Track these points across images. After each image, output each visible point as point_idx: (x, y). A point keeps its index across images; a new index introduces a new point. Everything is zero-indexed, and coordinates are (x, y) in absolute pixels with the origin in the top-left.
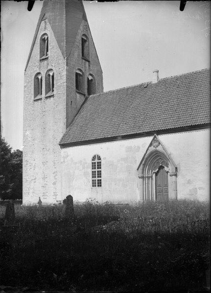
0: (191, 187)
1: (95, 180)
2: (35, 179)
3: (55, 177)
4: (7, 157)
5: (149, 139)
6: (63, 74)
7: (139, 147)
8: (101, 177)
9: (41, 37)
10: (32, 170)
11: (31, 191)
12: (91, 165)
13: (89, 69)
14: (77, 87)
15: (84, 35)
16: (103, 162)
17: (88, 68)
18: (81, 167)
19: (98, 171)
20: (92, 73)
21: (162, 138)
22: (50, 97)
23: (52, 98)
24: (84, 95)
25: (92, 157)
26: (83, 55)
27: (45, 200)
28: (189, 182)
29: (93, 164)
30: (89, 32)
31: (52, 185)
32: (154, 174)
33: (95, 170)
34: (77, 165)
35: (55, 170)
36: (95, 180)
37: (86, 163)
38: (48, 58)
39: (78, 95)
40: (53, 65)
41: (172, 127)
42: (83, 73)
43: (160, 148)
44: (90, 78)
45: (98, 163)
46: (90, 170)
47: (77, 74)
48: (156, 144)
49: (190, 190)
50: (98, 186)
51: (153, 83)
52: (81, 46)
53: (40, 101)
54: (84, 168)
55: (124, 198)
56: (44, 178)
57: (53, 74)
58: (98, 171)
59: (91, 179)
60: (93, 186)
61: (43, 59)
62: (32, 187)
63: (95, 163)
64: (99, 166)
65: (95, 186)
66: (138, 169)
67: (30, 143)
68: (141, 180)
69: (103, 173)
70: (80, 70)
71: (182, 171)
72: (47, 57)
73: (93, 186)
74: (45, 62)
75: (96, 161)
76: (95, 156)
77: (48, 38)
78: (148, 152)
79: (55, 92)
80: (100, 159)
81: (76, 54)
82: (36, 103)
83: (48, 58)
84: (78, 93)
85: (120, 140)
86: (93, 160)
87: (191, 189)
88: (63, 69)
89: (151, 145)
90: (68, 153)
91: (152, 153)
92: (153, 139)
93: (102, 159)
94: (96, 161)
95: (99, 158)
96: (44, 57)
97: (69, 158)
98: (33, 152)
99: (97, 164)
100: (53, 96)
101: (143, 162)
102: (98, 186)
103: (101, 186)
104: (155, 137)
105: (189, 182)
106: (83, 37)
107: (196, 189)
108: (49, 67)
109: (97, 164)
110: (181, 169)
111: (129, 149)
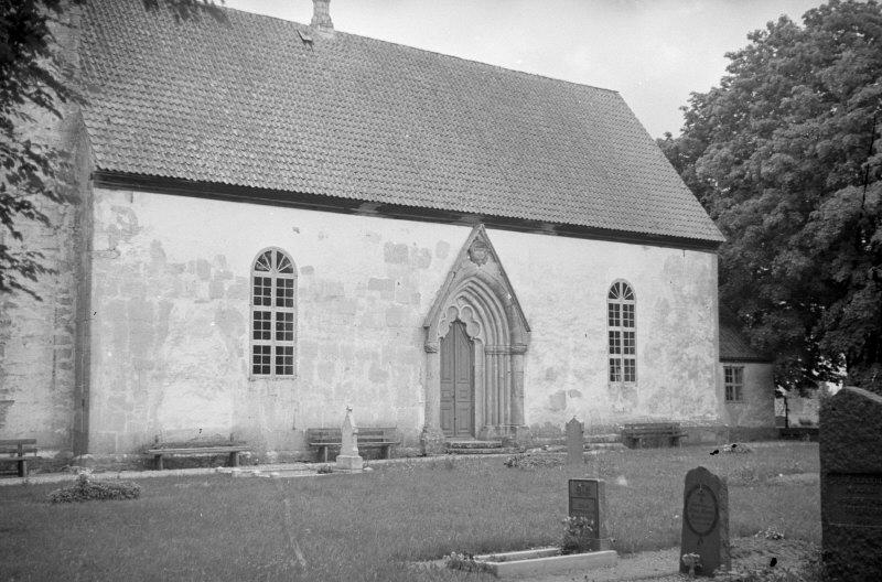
4: (799, 278)
8: (290, 337)
12: (249, 287)
16: (301, 282)
18: (204, 290)
21: (496, 237)
25: (607, 290)
34: (184, 276)
37: (229, 276)
41: (621, 229)
46: (245, 308)
49: (551, 396)
50: (279, 371)
54: (216, 293)
59: (247, 342)
60: (256, 370)
64: (286, 293)
65: (267, 370)
73: (256, 370)
75: (621, 301)
76: (617, 285)
80: (631, 298)
85: (368, 214)
86: (611, 296)
87: (553, 393)
95: (283, 261)
99: (273, 287)
102: (279, 371)
103: (289, 371)
105: (550, 376)
107: (564, 393)
109: (273, 287)
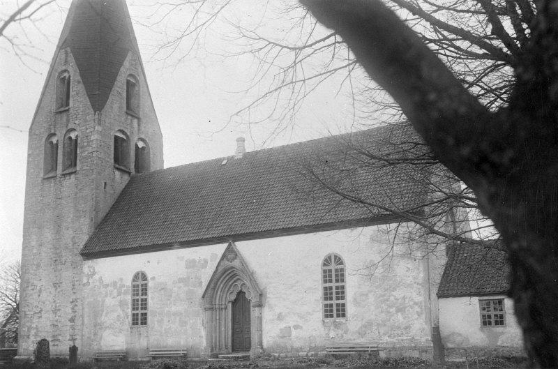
0: (283, 325)
1: (142, 309)
2: (40, 312)
3: (73, 309)
5: (220, 249)
6: (92, 138)
7: (206, 262)
9: (59, 76)
10: (35, 296)
11: (33, 332)
13: (139, 130)
14: (116, 160)
15: (130, 75)
16: (150, 284)
17: (136, 129)
19: (337, 288)
20: (143, 136)
21: (241, 246)
22: (70, 174)
23: (73, 176)
24: (129, 173)
26: (128, 107)
27: (55, 348)
28: (280, 317)
29: (327, 276)
30: (140, 70)
31: (68, 322)
32: (230, 304)
33: (137, 297)
34: (110, 288)
35: (74, 297)
36: (142, 309)
37: (123, 286)
38: (68, 110)
39: (117, 173)
40: (77, 122)
42: (127, 136)
43: (236, 263)
44: (141, 145)
45: (336, 270)
47: (116, 138)
48: (232, 256)
49: (281, 329)
50: (142, 323)
51: (236, 158)
52: (125, 95)
53: (53, 181)
54: (119, 294)
55: (182, 343)
56: (55, 311)
57: (58, 141)
58: (337, 288)
60: (327, 316)
61: (61, 112)
62: (34, 326)
63: (330, 271)
65: (137, 324)
66: (203, 297)
67: (35, 251)
68: (210, 312)
69: (150, 302)
70: (121, 131)
71: (271, 298)
72: (67, 108)
74: (64, 116)
75: (333, 267)
77: (70, 76)
78: (220, 269)
79: (78, 168)
80: (342, 263)
81: (116, 106)
82: (47, 184)
83: (68, 110)
84: (118, 169)
87: (282, 327)
88: (92, 130)
89: (224, 256)
90: (94, 269)
91: (225, 271)
92: (228, 249)
93: (149, 278)
94: (333, 267)
96: (63, 109)
97: (96, 277)
98: (38, 266)
99: (333, 272)
100: (75, 172)
101: (212, 285)
103: (146, 323)
104: (230, 245)
105: (280, 317)
106: (129, 79)
108: (71, 126)
110: (268, 296)
111: (191, 264)
